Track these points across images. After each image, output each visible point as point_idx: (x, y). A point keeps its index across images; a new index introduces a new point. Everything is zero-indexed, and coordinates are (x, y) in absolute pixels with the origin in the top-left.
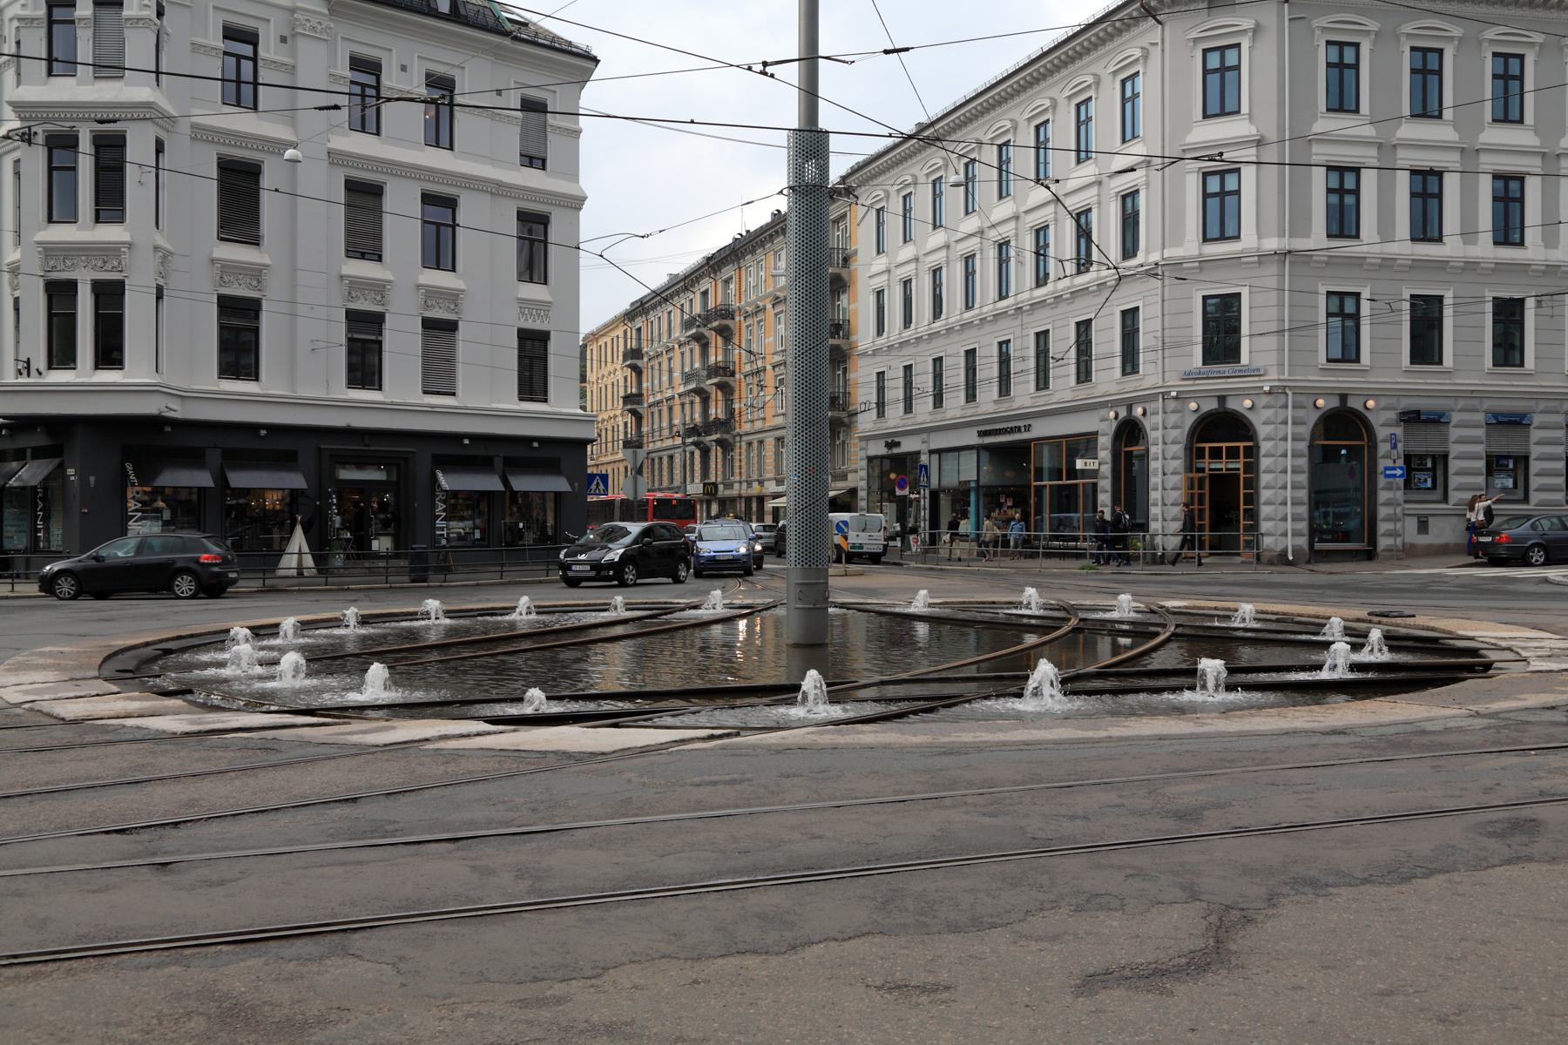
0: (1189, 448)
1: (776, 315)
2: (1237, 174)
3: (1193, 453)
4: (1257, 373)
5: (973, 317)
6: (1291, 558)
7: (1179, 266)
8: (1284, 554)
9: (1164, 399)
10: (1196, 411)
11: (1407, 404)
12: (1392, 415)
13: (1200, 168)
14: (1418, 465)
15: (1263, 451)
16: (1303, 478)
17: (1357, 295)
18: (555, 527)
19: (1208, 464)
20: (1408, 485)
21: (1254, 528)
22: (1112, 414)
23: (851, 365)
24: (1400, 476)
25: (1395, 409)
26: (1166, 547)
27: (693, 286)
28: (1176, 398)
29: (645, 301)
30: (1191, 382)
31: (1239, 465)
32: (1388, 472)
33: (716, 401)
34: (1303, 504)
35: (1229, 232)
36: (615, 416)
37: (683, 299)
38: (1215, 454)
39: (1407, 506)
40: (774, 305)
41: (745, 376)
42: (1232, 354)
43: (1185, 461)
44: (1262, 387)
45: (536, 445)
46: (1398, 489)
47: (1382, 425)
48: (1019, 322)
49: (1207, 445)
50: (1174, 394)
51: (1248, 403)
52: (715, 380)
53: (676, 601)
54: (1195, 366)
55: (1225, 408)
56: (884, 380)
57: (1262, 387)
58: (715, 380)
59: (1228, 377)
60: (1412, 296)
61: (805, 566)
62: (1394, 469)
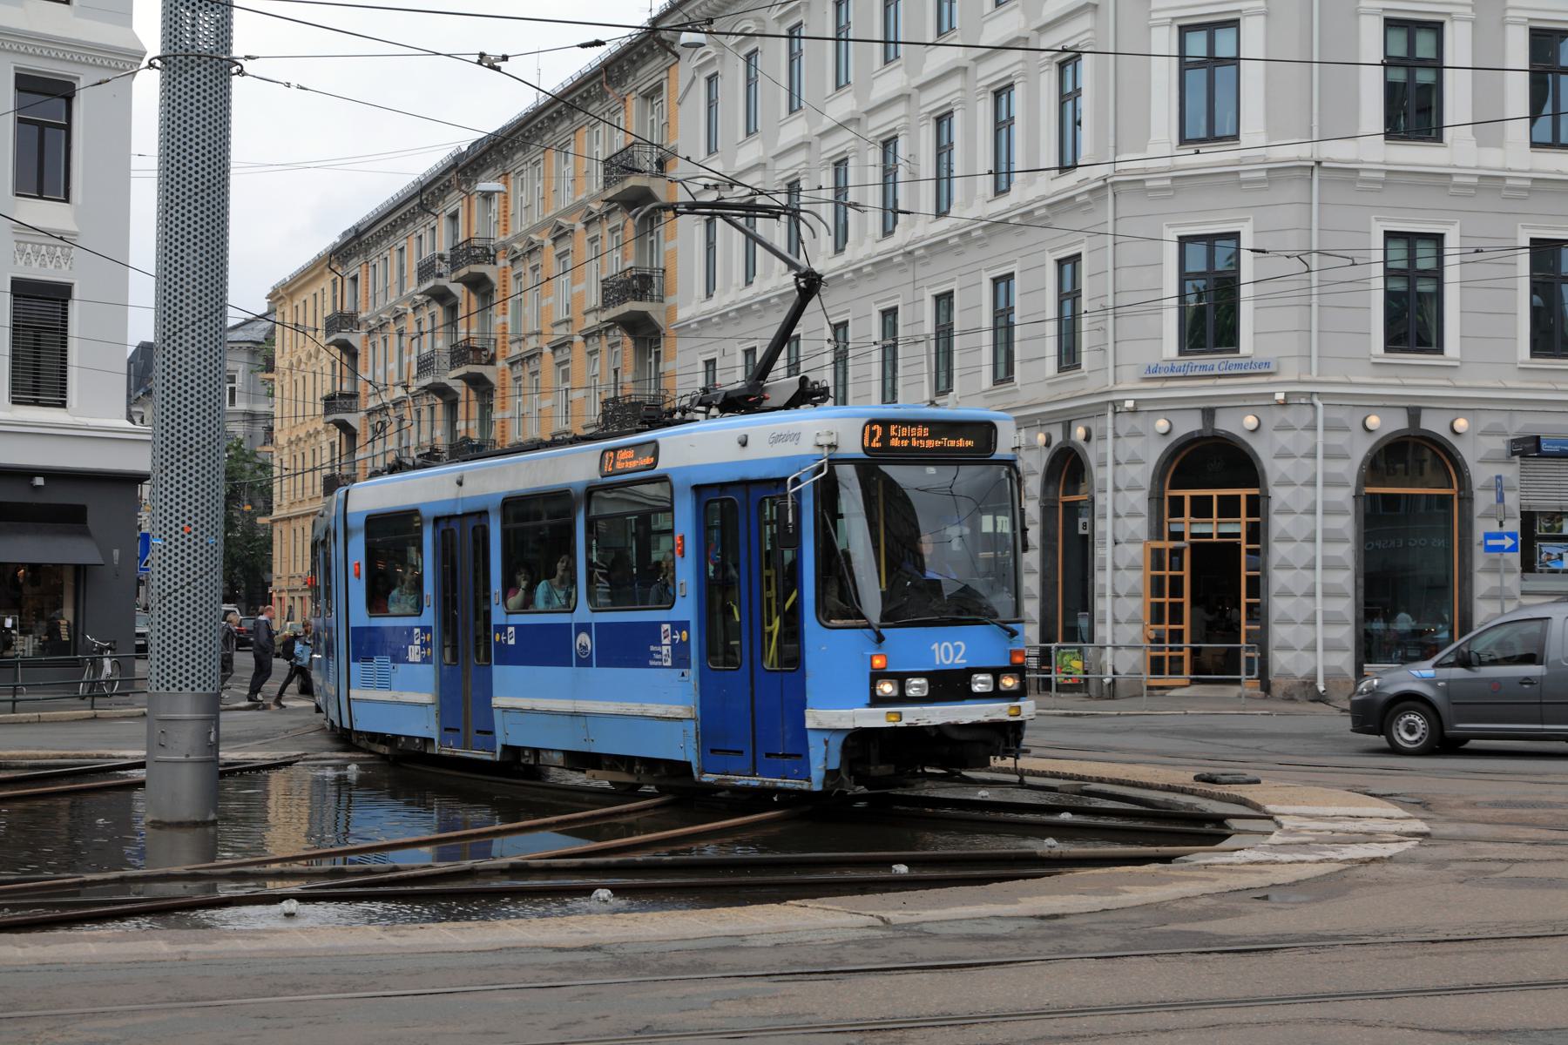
0: (1156, 498)
1: (560, 256)
2: (1234, 30)
3: (1164, 507)
4: (1264, 370)
5: (843, 267)
6: (1321, 688)
7: (1139, 186)
8: (1310, 682)
9: (1115, 413)
10: (1455, 433)
11: (1524, 424)
12: (1499, 444)
13: (1174, 19)
14: (1547, 529)
15: (1274, 505)
16: (1346, 551)
17: (1438, 239)
18: (75, 628)
19: (1189, 525)
20: (1528, 566)
21: (1261, 641)
22: (1041, 438)
23: (664, 345)
24: (1512, 549)
25: (1504, 434)
26: (1118, 669)
27: (434, 204)
28: (1134, 411)
29: (362, 229)
30: (1157, 385)
31: (1239, 526)
32: (1491, 542)
33: (468, 401)
34: (1344, 595)
35: (1224, 126)
36: (318, 432)
37: (420, 227)
38: (1201, 508)
39: (1527, 601)
40: (555, 240)
41: (512, 364)
42: (1227, 337)
43: (1150, 523)
44: (1274, 394)
45: (39, 481)
46: (1511, 571)
47: (1483, 461)
48: (908, 277)
49: (1187, 494)
50: (1129, 404)
51: (1250, 421)
52: (462, 371)
53: (122, 753)
54: (1165, 356)
55: (1213, 430)
56: (714, 370)
57: (1274, 394)
58: (462, 371)
59: (1220, 376)
60: (1532, 240)
61: (198, 690)
62: (1500, 536)
